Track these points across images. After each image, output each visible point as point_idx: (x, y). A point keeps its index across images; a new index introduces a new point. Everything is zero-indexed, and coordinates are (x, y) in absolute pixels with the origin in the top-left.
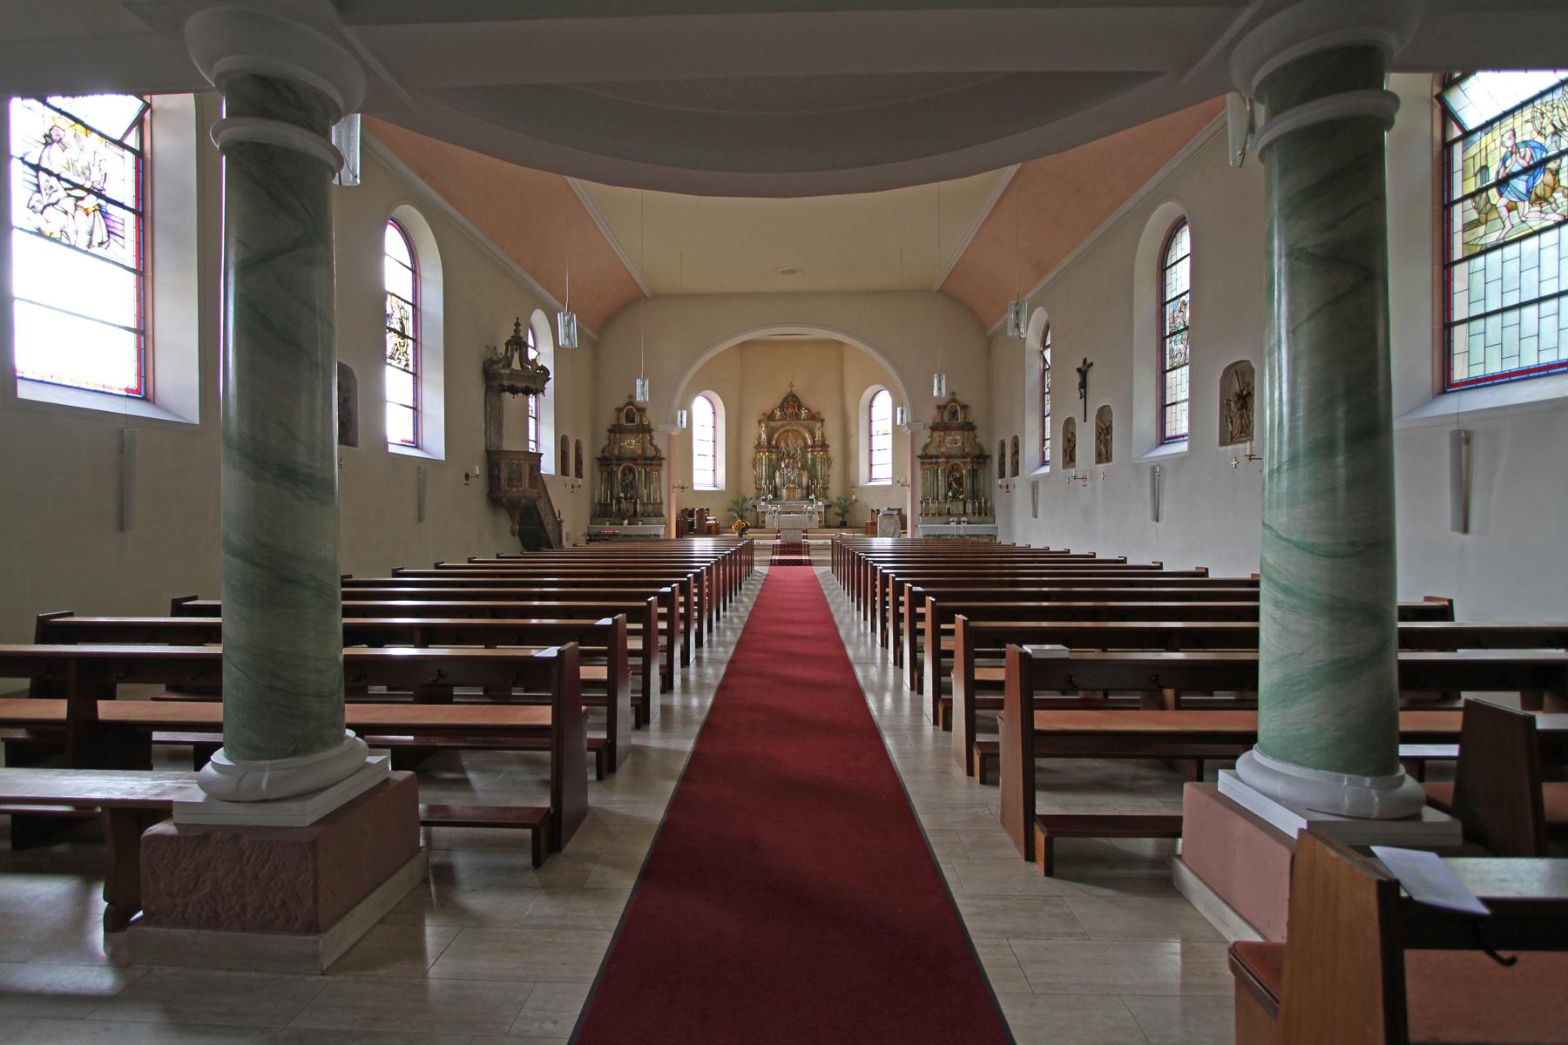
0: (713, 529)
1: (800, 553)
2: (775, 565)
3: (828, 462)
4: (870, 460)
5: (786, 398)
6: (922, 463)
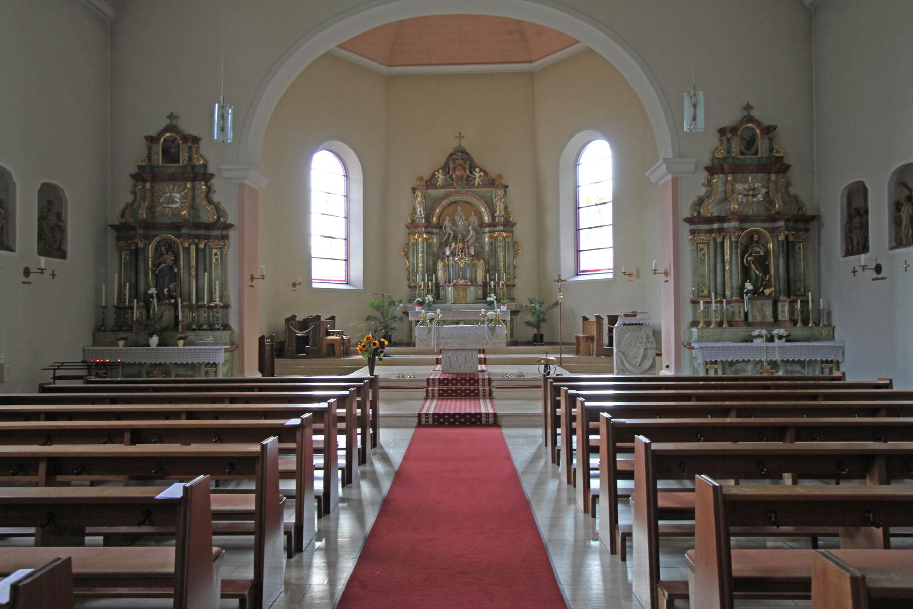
0: (338, 349)
1: (474, 395)
2: (427, 425)
3: (514, 247)
4: (577, 244)
5: (451, 155)
6: (693, 232)
